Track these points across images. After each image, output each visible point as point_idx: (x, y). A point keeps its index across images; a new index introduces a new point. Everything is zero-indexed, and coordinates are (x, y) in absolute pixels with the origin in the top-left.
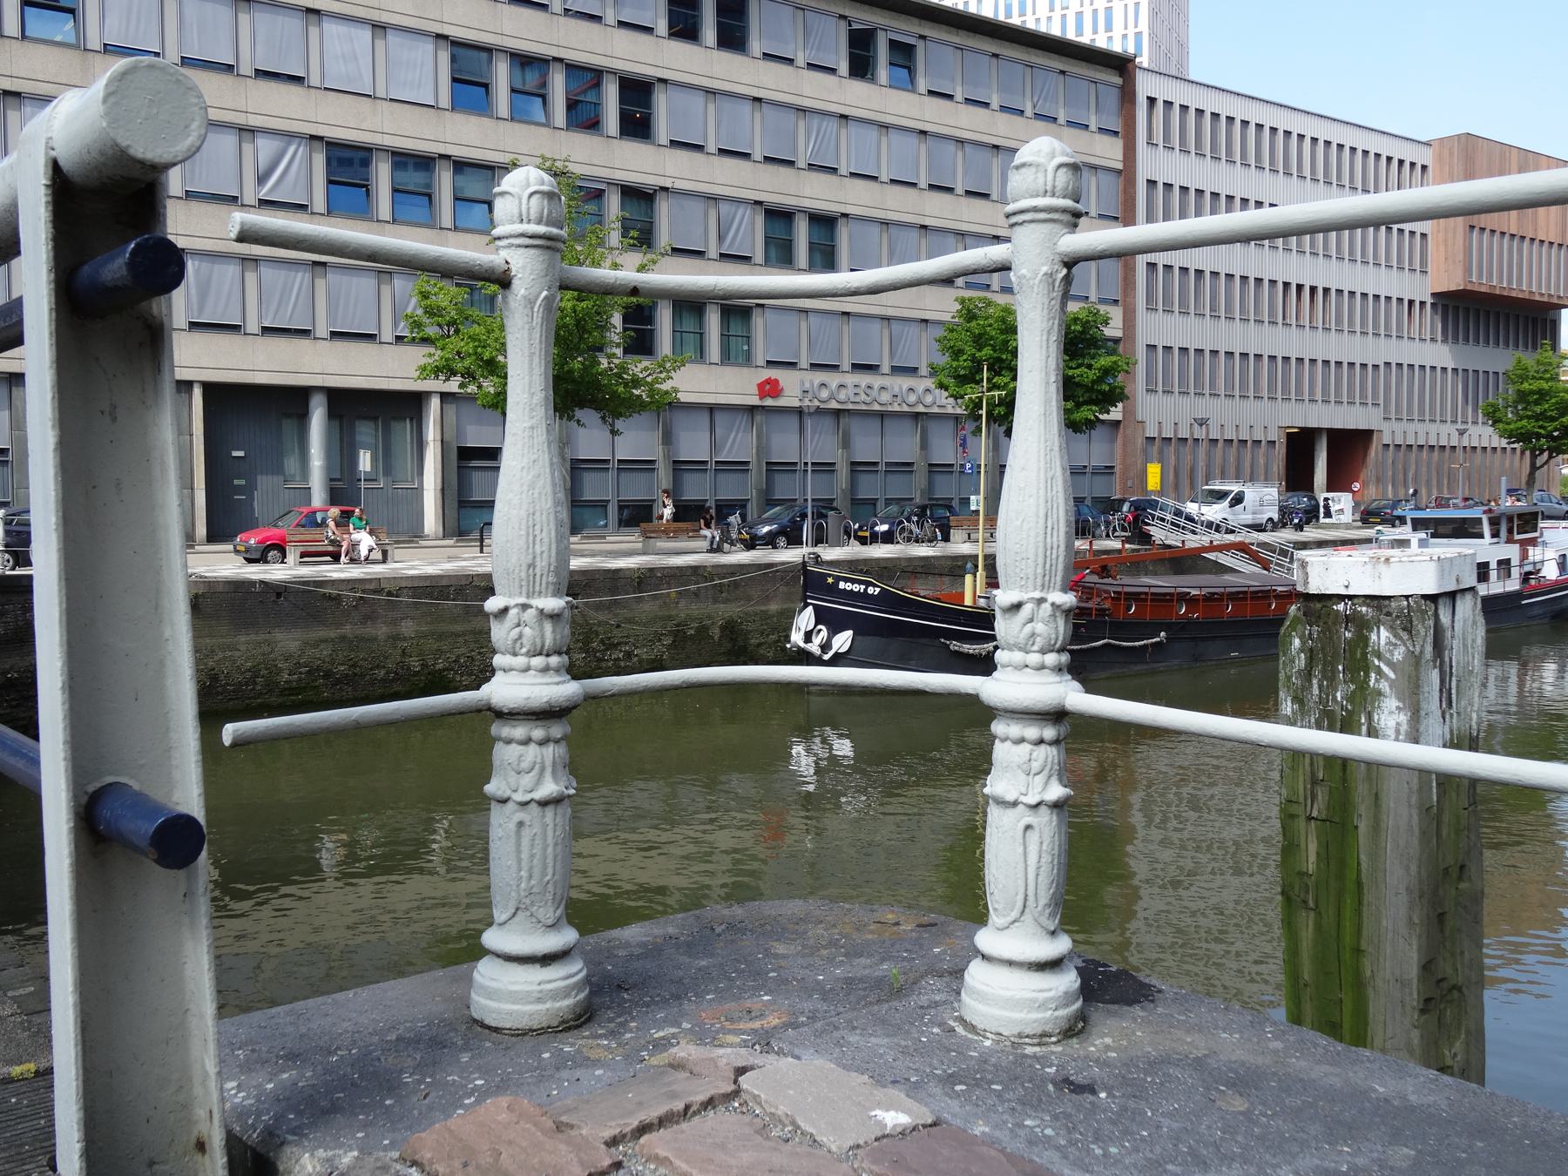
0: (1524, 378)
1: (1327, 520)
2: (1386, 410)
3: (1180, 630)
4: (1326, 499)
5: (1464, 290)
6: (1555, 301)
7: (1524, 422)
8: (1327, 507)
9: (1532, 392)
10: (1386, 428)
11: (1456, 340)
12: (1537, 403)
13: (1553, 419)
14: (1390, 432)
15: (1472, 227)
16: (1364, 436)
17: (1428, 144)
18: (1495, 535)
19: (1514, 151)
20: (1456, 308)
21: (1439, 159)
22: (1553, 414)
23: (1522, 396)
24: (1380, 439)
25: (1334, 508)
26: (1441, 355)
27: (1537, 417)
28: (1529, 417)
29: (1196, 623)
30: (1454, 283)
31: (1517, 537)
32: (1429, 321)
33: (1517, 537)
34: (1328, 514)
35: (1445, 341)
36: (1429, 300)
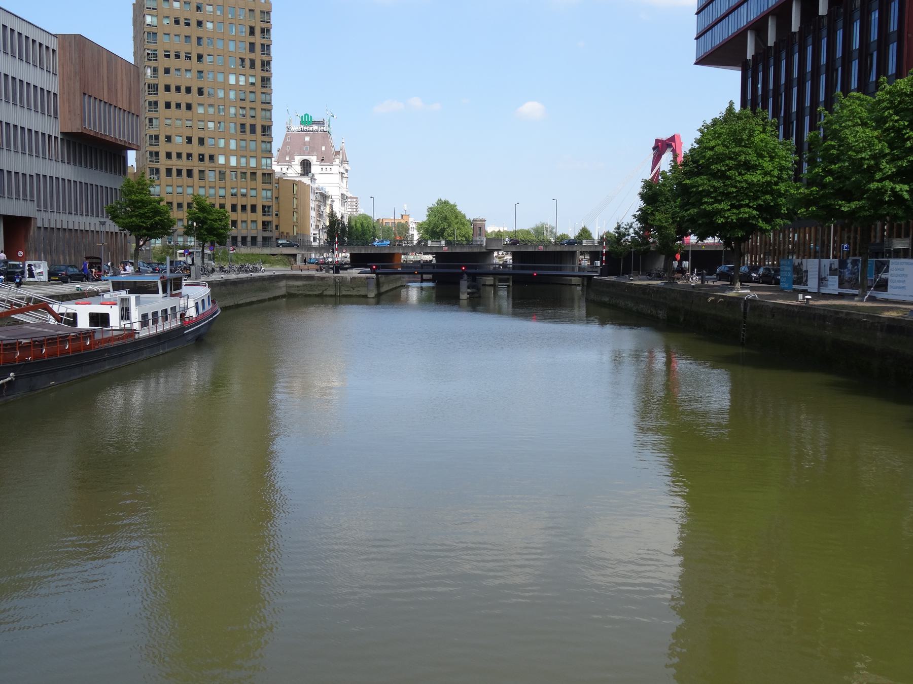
0: (131, 193)
1: (31, 279)
2: (39, 205)
3: (22, 368)
4: (30, 265)
5: (82, 133)
6: (127, 145)
7: (134, 219)
8: (30, 271)
9: (138, 201)
10: (38, 215)
11: (75, 164)
12: (140, 208)
13: (148, 218)
14: (43, 219)
15: (85, 94)
16: (26, 221)
17: (55, 36)
18: (165, 291)
19: (105, 52)
20: (74, 143)
21: (62, 47)
22: (150, 215)
23: (132, 203)
24: (36, 223)
25: (36, 271)
26: (65, 171)
27: (141, 216)
28: (136, 216)
29: (29, 364)
30: (75, 127)
31: (174, 292)
32: (58, 148)
33: (174, 292)
34: (31, 275)
35: (69, 163)
36: (60, 136)
